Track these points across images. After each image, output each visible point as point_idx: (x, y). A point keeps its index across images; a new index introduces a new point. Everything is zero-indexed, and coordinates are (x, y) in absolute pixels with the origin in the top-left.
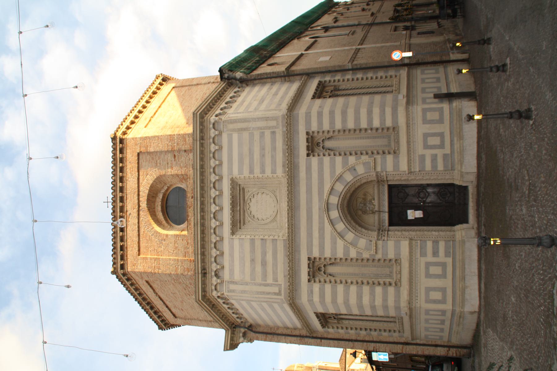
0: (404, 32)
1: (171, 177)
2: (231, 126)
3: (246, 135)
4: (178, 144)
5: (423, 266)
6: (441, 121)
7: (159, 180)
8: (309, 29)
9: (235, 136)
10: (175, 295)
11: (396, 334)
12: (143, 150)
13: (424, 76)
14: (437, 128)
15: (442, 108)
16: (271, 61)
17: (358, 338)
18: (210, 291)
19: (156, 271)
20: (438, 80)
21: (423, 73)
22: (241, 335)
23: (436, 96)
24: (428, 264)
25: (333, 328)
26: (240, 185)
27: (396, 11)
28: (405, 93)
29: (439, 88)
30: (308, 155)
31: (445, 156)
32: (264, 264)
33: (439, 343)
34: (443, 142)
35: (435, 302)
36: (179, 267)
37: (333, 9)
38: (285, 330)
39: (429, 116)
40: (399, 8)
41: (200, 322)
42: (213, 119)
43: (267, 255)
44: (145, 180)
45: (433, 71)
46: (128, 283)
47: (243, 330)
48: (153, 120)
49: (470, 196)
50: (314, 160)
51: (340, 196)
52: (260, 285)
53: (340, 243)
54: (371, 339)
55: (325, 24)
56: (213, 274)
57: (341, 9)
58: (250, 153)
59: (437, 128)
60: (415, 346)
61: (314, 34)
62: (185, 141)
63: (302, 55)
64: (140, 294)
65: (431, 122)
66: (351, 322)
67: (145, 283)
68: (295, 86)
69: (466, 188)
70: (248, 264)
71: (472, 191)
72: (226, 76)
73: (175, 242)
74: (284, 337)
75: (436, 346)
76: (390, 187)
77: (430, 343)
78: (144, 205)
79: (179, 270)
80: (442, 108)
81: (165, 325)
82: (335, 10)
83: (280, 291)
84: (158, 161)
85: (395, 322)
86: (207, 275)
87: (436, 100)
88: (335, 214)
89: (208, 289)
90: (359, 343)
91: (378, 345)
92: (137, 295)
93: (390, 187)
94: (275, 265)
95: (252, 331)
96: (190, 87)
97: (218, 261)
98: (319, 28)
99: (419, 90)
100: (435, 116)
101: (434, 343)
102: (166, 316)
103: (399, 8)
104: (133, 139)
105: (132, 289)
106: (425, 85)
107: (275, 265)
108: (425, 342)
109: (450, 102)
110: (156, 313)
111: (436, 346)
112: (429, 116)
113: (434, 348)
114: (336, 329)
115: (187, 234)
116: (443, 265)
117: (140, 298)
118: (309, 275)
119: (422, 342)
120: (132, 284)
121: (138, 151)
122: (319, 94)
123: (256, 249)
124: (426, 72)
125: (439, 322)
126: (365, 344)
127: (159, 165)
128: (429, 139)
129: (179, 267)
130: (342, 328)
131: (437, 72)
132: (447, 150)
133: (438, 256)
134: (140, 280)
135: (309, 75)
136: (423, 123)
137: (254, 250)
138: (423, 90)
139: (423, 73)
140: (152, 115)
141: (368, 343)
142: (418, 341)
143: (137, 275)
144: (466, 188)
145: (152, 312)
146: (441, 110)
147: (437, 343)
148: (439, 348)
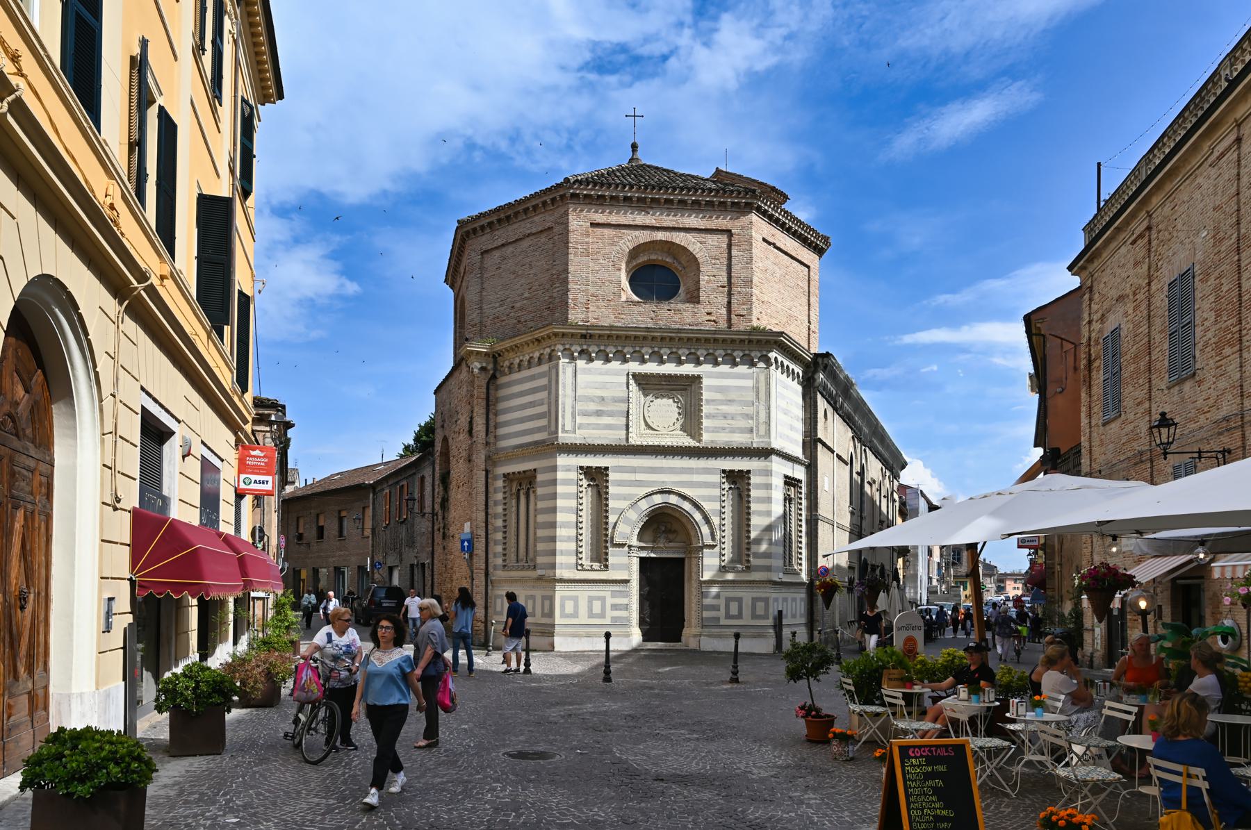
0: (847, 580)
1: (697, 280)
2: (762, 378)
3: (750, 396)
4: (740, 292)
5: (602, 594)
6: (754, 616)
7: (694, 262)
8: (863, 447)
9: (749, 383)
10: (528, 266)
11: (499, 561)
12: (735, 239)
13: (798, 601)
14: (747, 612)
15: (768, 618)
16: (830, 411)
17: (489, 516)
18: (563, 342)
19: (571, 250)
20: (794, 616)
21: (801, 599)
22: (484, 365)
23: (780, 612)
24: (603, 599)
25: (504, 487)
26: (691, 385)
27: (874, 568)
28: (783, 580)
29: (786, 617)
30: (724, 471)
31: (718, 619)
32: (599, 413)
33: (490, 611)
34: (733, 617)
35: (563, 606)
36: (579, 287)
37: (888, 474)
38: (494, 424)
39: (760, 605)
40: (878, 572)
41: (478, 291)
42: (772, 355)
43: (610, 418)
44: (693, 240)
45: (803, 611)
46: (548, 199)
47: (490, 367)
48: (771, 247)
49: (672, 644)
50: (716, 478)
51: (677, 506)
52: (574, 408)
53: (624, 504)
54: (489, 532)
55: (867, 469)
56: (585, 347)
57: (888, 485)
58: (730, 401)
59: (747, 612)
60: (484, 583)
61: (856, 458)
62: (743, 304)
63: (833, 452)
64: (526, 210)
65: (754, 607)
66: (514, 509)
67: (549, 224)
68: (798, 452)
69: (679, 641)
70: (599, 393)
71: (677, 646)
72: (820, 360)
73: (611, 282)
74: (485, 422)
75: (486, 608)
76: (682, 561)
77: (489, 601)
78: (660, 236)
79: (575, 287)
80: (768, 618)
81: (468, 233)
82: (887, 477)
83: (567, 431)
84: (718, 262)
85: (517, 561)
86: (583, 340)
87: (776, 613)
88: (658, 499)
89: (565, 340)
90: (484, 517)
91: (483, 540)
92: (527, 206)
93: (682, 561)
94: (597, 426)
95: (490, 379)
96: (807, 294)
97: (600, 354)
98: (864, 461)
99: (785, 595)
100: (760, 611)
101: (489, 604)
102: (484, 238)
103: (878, 572)
104: (751, 223)
105: (538, 201)
106: (780, 601)
107: (597, 426)
108: (489, 595)
109: (775, 627)
110: (491, 224)
111: (486, 608)
112: (760, 605)
113: (484, 605)
114: (503, 490)
115: (622, 300)
116: (602, 615)
117: (521, 208)
118: (588, 467)
119: (489, 591)
120: (544, 203)
121: (733, 231)
122: (790, 482)
123: (617, 404)
124: (803, 603)
125: (785, 604)
126: (484, 525)
127: (713, 262)
128: (572, 603)
129: (579, 287)
130: (505, 498)
131: (801, 616)
132: (723, 622)
133: (719, 606)
134: (552, 218)
135: (812, 468)
136: (753, 598)
137: (616, 401)
138: (785, 600)
139: (801, 599)
140: (778, 244)
141: (484, 529)
142: (490, 587)
143: (561, 217)
144: (679, 641)
145: (494, 218)
146: (766, 617)
147: (489, 609)
148: (483, 611)
